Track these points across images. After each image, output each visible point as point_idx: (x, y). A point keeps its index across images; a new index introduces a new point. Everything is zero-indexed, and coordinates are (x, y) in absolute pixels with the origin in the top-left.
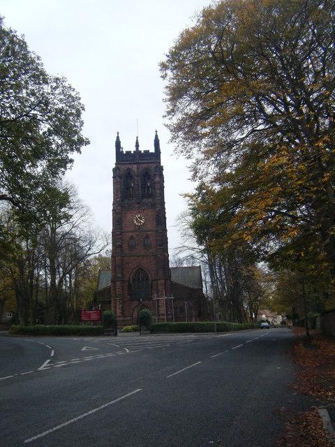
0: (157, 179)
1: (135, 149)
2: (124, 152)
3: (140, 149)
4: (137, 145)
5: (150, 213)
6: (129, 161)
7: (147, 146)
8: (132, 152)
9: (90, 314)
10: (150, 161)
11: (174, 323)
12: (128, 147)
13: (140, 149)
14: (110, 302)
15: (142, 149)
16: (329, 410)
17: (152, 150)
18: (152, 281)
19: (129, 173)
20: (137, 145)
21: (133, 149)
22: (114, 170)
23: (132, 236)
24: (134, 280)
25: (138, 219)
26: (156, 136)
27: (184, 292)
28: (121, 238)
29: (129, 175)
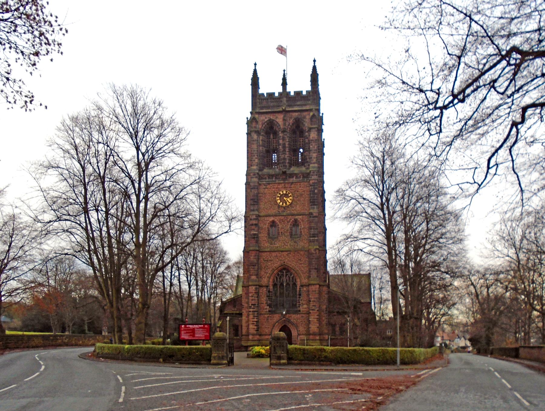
0: (313, 135)
1: (280, 90)
2: (292, 94)
3: (288, 90)
4: (284, 83)
5: (303, 188)
6: (268, 107)
7: (300, 84)
8: (304, 93)
9: (193, 330)
10: (304, 108)
11: (349, 348)
12: (270, 86)
13: (288, 90)
14: (241, 315)
15: (291, 89)
16: (126, 388)
17: (305, 87)
18: (302, 286)
19: (271, 128)
20: (284, 83)
21: (277, 89)
22: (250, 123)
23: (273, 222)
24: (275, 285)
25: (284, 197)
26: (255, 72)
27: (347, 299)
28: (256, 225)
29: (271, 129)
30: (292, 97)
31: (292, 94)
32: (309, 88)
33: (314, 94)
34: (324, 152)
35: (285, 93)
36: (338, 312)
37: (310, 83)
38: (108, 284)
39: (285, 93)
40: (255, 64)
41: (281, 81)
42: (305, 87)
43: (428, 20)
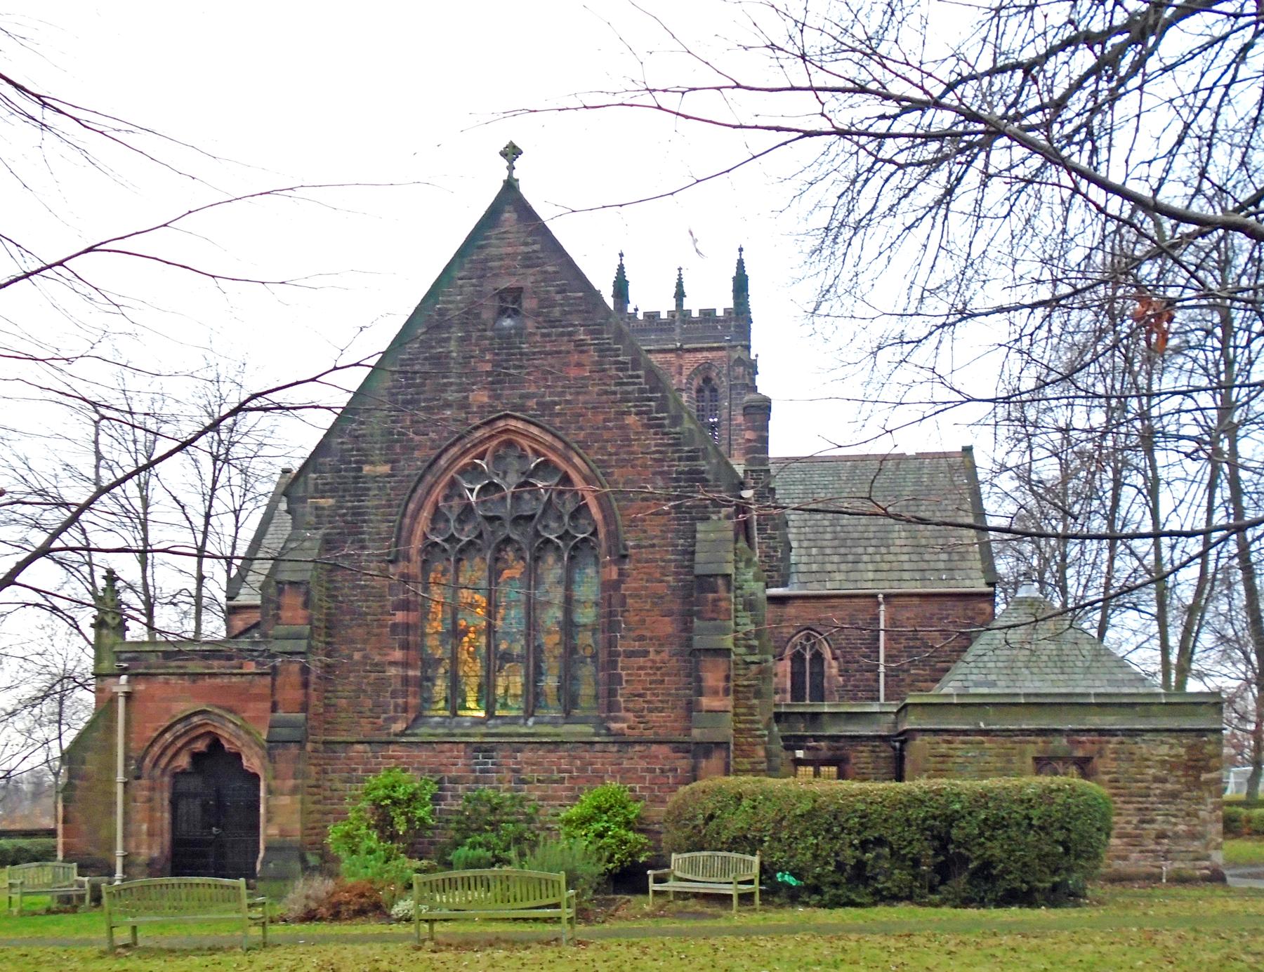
2: (695, 314)
4: (680, 295)
6: (698, 340)
15: (693, 305)
17: (722, 301)
20: (680, 295)
21: (665, 306)
26: (740, 263)
30: (695, 321)
31: (695, 314)
32: (730, 304)
33: (741, 314)
34: (765, 385)
35: (680, 314)
36: (210, 949)
37: (731, 295)
38: (1180, 655)
39: (680, 314)
40: (741, 250)
41: (674, 290)
42: (722, 301)
43: (1055, 262)
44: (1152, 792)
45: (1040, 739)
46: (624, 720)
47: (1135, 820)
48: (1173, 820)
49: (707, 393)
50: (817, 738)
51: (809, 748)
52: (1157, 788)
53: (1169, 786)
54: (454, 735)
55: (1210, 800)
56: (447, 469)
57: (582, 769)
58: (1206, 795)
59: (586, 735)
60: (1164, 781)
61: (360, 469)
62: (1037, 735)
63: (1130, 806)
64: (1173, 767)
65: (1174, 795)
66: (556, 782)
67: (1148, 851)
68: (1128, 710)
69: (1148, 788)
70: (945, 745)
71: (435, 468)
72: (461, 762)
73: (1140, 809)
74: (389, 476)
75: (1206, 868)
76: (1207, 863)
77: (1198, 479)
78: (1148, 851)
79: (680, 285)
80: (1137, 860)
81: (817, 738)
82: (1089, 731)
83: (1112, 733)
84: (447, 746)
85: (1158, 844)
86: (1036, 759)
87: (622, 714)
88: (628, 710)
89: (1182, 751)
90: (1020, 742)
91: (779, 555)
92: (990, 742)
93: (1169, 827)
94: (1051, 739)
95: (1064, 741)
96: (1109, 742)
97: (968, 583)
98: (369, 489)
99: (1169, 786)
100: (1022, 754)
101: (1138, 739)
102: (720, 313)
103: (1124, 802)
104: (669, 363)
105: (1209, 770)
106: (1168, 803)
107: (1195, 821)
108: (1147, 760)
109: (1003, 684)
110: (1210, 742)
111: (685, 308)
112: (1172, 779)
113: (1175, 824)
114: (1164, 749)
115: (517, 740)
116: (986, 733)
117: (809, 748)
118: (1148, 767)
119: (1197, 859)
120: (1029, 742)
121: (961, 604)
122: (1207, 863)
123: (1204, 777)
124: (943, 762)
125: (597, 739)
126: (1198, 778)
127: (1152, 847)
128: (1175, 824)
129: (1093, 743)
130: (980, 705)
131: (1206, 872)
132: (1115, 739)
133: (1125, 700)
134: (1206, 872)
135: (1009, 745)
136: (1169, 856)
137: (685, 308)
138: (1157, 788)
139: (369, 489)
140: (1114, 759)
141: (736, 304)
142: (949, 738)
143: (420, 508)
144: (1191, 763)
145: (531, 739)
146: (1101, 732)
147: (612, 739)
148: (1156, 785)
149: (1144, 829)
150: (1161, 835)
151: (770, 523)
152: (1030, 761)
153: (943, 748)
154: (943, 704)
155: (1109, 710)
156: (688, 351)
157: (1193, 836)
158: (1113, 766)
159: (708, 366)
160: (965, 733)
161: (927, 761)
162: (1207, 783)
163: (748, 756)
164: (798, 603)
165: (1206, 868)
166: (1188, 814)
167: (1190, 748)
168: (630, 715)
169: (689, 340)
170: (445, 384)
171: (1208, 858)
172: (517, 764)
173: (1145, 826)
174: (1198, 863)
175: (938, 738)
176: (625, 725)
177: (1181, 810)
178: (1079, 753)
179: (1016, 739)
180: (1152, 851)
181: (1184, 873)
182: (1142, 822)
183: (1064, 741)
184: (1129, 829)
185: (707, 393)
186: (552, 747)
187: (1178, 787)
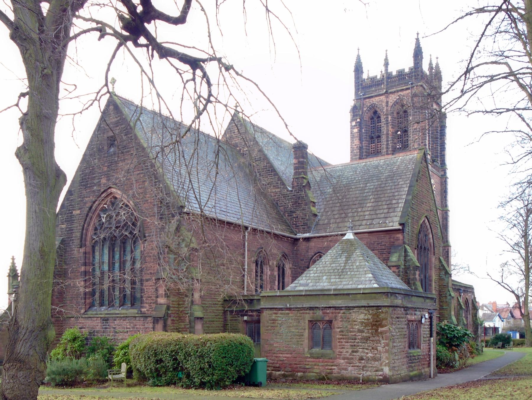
2: (394, 73)
4: (386, 64)
15: (393, 70)
20: (386, 64)
35: (389, 76)
41: (383, 62)
44: (357, 337)
45: (311, 312)
46: (145, 307)
47: (350, 351)
48: (366, 351)
49: (375, 119)
50: (252, 311)
51: (249, 316)
52: (359, 336)
53: (364, 334)
54: (97, 314)
55: (382, 341)
56: (96, 210)
57: (133, 328)
58: (381, 339)
59: (134, 313)
60: (362, 331)
61: (72, 213)
62: (310, 310)
63: (348, 344)
64: (367, 325)
65: (367, 339)
66: (125, 333)
67: (355, 366)
68: (347, 297)
69: (355, 335)
70: (274, 315)
71: (92, 210)
72: (100, 324)
73: (352, 346)
74: (80, 214)
75: (380, 375)
76: (381, 373)
77: (228, 208)
78: (355, 366)
79: (386, 60)
80: (351, 371)
81: (252, 311)
82: (330, 307)
83: (340, 308)
84: (95, 318)
85: (360, 363)
86: (310, 321)
87: (145, 305)
88: (146, 303)
89: (370, 317)
90: (303, 313)
91: (307, 217)
92: (292, 313)
93: (364, 354)
94: (315, 311)
95: (321, 312)
96: (339, 313)
97: (391, 224)
98: (74, 220)
99: (364, 334)
100: (304, 319)
101: (351, 311)
102: (407, 70)
103: (346, 342)
104: (382, 101)
105: (382, 327)
106: (364, 343)
107: (376, 352)
108: (355, 321)
109: (311, 284)
110: (382, 312)
111: (389, 71)
112: (366, 331)
113: (367, 353)
114: (362, 316)
115: (114, 316)
116: (290, 309)
117: (249, 316)
118: (355, 325)
119: (377, 371)
120: (306, 313)
121: (388, 236)
122: (381, 373)
123: (380, 330)
124: (273, 323)
125: (137, 315)
126: (377, 330)
127: (358, 364)
128: (367, 353)
129: (332, 313)
130: (288, 296)
131: (381, 377)
132: (342, 311)
133: (345, 292)
134: (381, 377)
135: (299, 315)
136: (365, 369)
137: (389, 71)
138: (359, 336)
139: (74, 220)
140: (341, 321)
141: (415, 64)
142: (276, 312)
143: (89, 225)
144: (374, 323)
145: (118, 316)
146: (335, 308)
147: (141, 315)
148: (359, 334)
149: (353, 355)
150: (361, 359)
151: (303, 202)
152: (307, 322)
153: (274, 316)
154: (273, 296)
155: (338, 297)
156: (391, 93)
157: (375, 359)
158: (340, 324)
159: (401, 99)
160: (281, 309)
161: (268, 322)
162: (381, 333)
163: (183, 322)
164: (315, 240)
165: (380, 375)
166: (373, 348)
167: (373, 315)
168: (147, 305)
169: (392, 87)
170: (94, 177)
171: (382, 370)
172: (115, 325)
173: (355, 354)
174: (377, 373)
175: (271, 312)
176: (146, 309)
177: (369, 346)
178: (327, 318)
179: (301, 312)
180: (357, 366)
181: (371, 377)
182: (353, 352)
183: (321, 312)
184: (348, 355)
185: (375, 119)
186: (124, 318)
187: (368, 335)
